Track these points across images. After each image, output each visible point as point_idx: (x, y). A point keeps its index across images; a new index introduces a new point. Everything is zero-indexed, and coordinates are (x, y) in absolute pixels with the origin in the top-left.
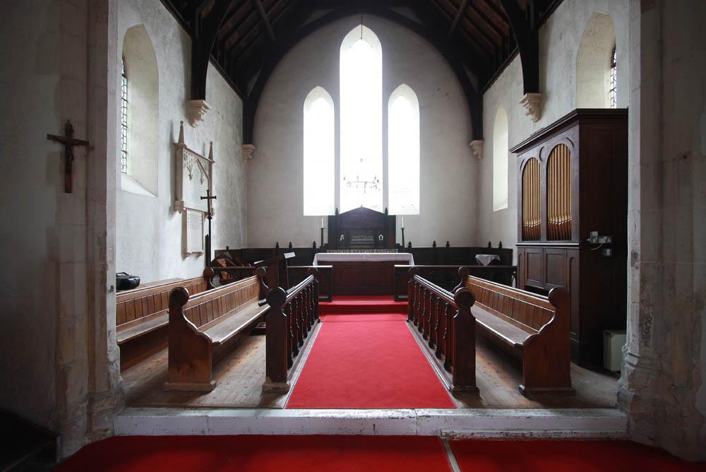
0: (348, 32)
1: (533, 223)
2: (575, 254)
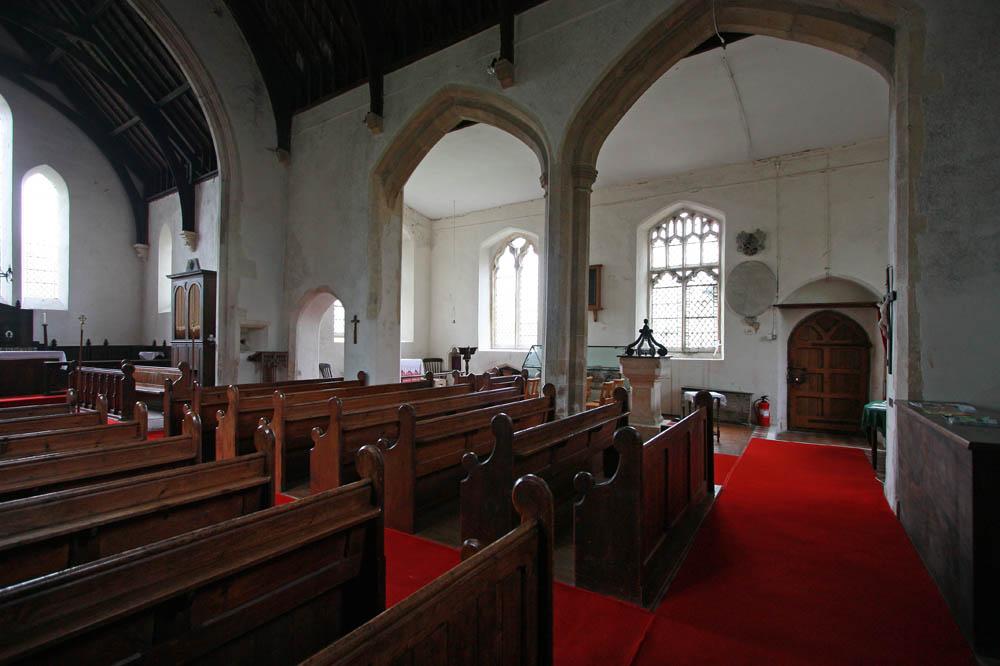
1: (181, 328)
2: (201, 346)
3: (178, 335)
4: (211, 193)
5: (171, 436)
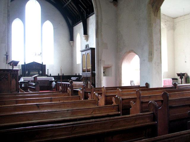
1: (84, 69)
3: (83, 71)
4: (92, 21)
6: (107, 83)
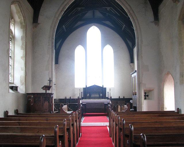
0: (89, 28)
5: (59, 136)
6: (148, 107)
